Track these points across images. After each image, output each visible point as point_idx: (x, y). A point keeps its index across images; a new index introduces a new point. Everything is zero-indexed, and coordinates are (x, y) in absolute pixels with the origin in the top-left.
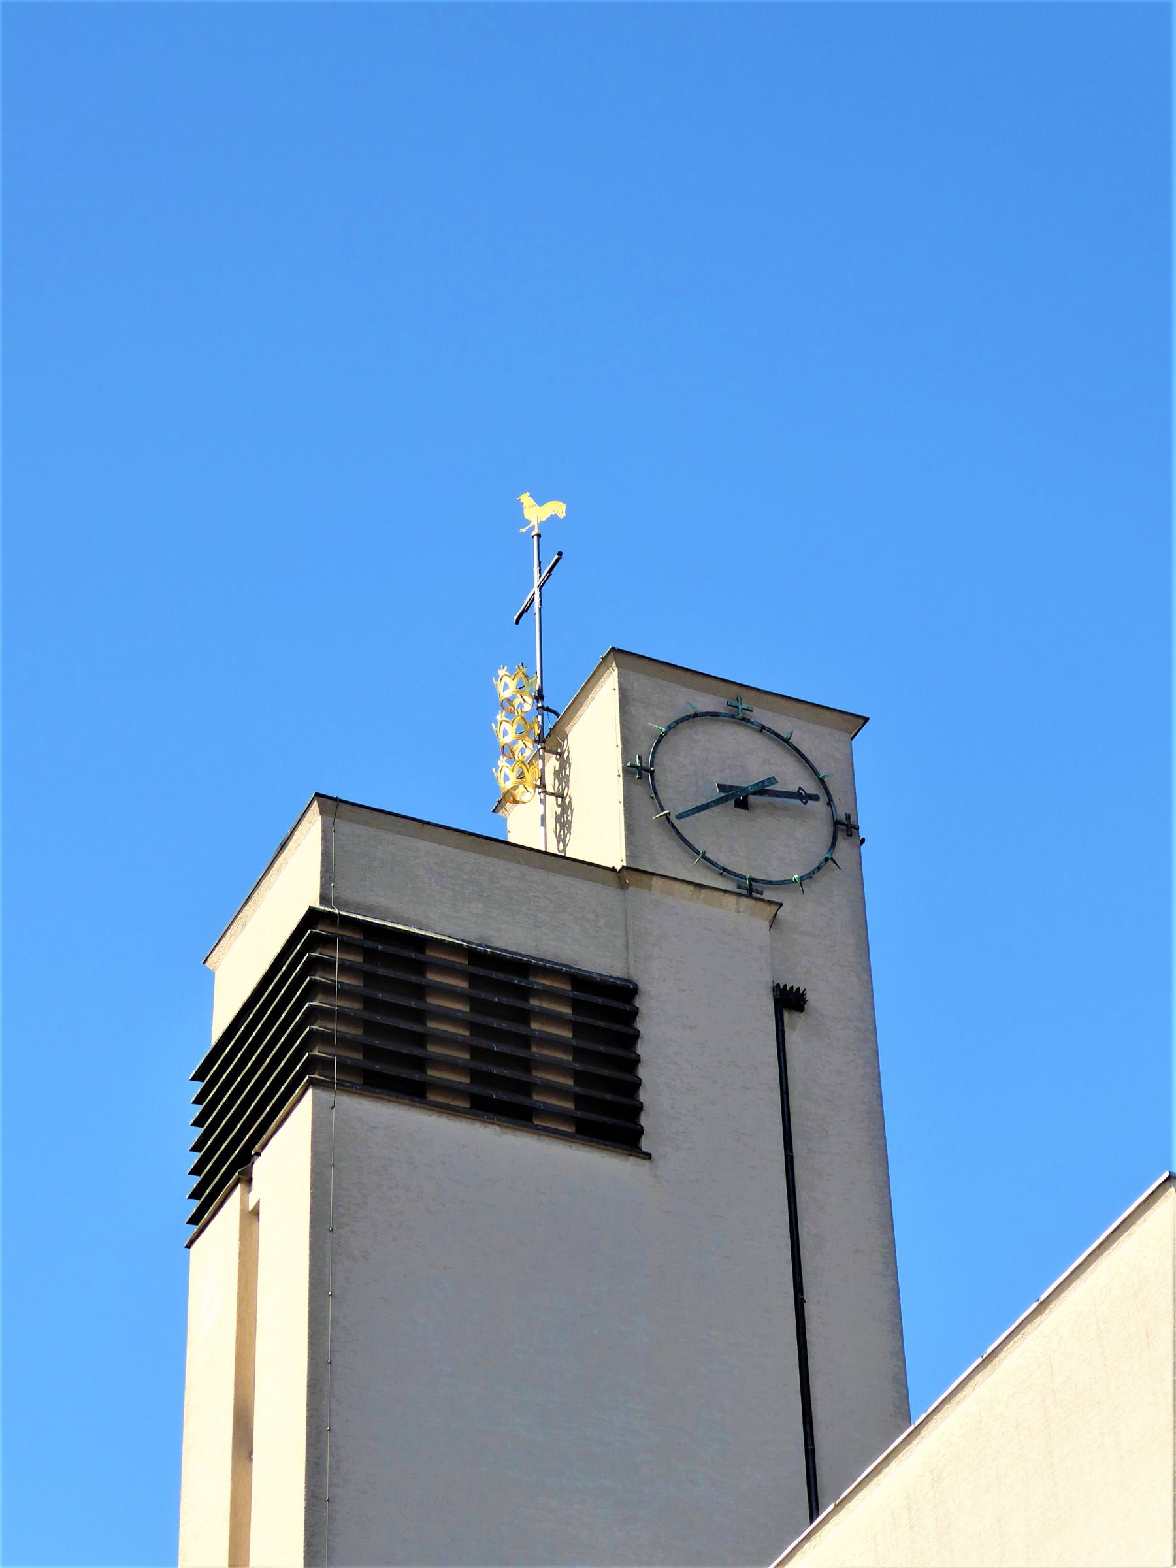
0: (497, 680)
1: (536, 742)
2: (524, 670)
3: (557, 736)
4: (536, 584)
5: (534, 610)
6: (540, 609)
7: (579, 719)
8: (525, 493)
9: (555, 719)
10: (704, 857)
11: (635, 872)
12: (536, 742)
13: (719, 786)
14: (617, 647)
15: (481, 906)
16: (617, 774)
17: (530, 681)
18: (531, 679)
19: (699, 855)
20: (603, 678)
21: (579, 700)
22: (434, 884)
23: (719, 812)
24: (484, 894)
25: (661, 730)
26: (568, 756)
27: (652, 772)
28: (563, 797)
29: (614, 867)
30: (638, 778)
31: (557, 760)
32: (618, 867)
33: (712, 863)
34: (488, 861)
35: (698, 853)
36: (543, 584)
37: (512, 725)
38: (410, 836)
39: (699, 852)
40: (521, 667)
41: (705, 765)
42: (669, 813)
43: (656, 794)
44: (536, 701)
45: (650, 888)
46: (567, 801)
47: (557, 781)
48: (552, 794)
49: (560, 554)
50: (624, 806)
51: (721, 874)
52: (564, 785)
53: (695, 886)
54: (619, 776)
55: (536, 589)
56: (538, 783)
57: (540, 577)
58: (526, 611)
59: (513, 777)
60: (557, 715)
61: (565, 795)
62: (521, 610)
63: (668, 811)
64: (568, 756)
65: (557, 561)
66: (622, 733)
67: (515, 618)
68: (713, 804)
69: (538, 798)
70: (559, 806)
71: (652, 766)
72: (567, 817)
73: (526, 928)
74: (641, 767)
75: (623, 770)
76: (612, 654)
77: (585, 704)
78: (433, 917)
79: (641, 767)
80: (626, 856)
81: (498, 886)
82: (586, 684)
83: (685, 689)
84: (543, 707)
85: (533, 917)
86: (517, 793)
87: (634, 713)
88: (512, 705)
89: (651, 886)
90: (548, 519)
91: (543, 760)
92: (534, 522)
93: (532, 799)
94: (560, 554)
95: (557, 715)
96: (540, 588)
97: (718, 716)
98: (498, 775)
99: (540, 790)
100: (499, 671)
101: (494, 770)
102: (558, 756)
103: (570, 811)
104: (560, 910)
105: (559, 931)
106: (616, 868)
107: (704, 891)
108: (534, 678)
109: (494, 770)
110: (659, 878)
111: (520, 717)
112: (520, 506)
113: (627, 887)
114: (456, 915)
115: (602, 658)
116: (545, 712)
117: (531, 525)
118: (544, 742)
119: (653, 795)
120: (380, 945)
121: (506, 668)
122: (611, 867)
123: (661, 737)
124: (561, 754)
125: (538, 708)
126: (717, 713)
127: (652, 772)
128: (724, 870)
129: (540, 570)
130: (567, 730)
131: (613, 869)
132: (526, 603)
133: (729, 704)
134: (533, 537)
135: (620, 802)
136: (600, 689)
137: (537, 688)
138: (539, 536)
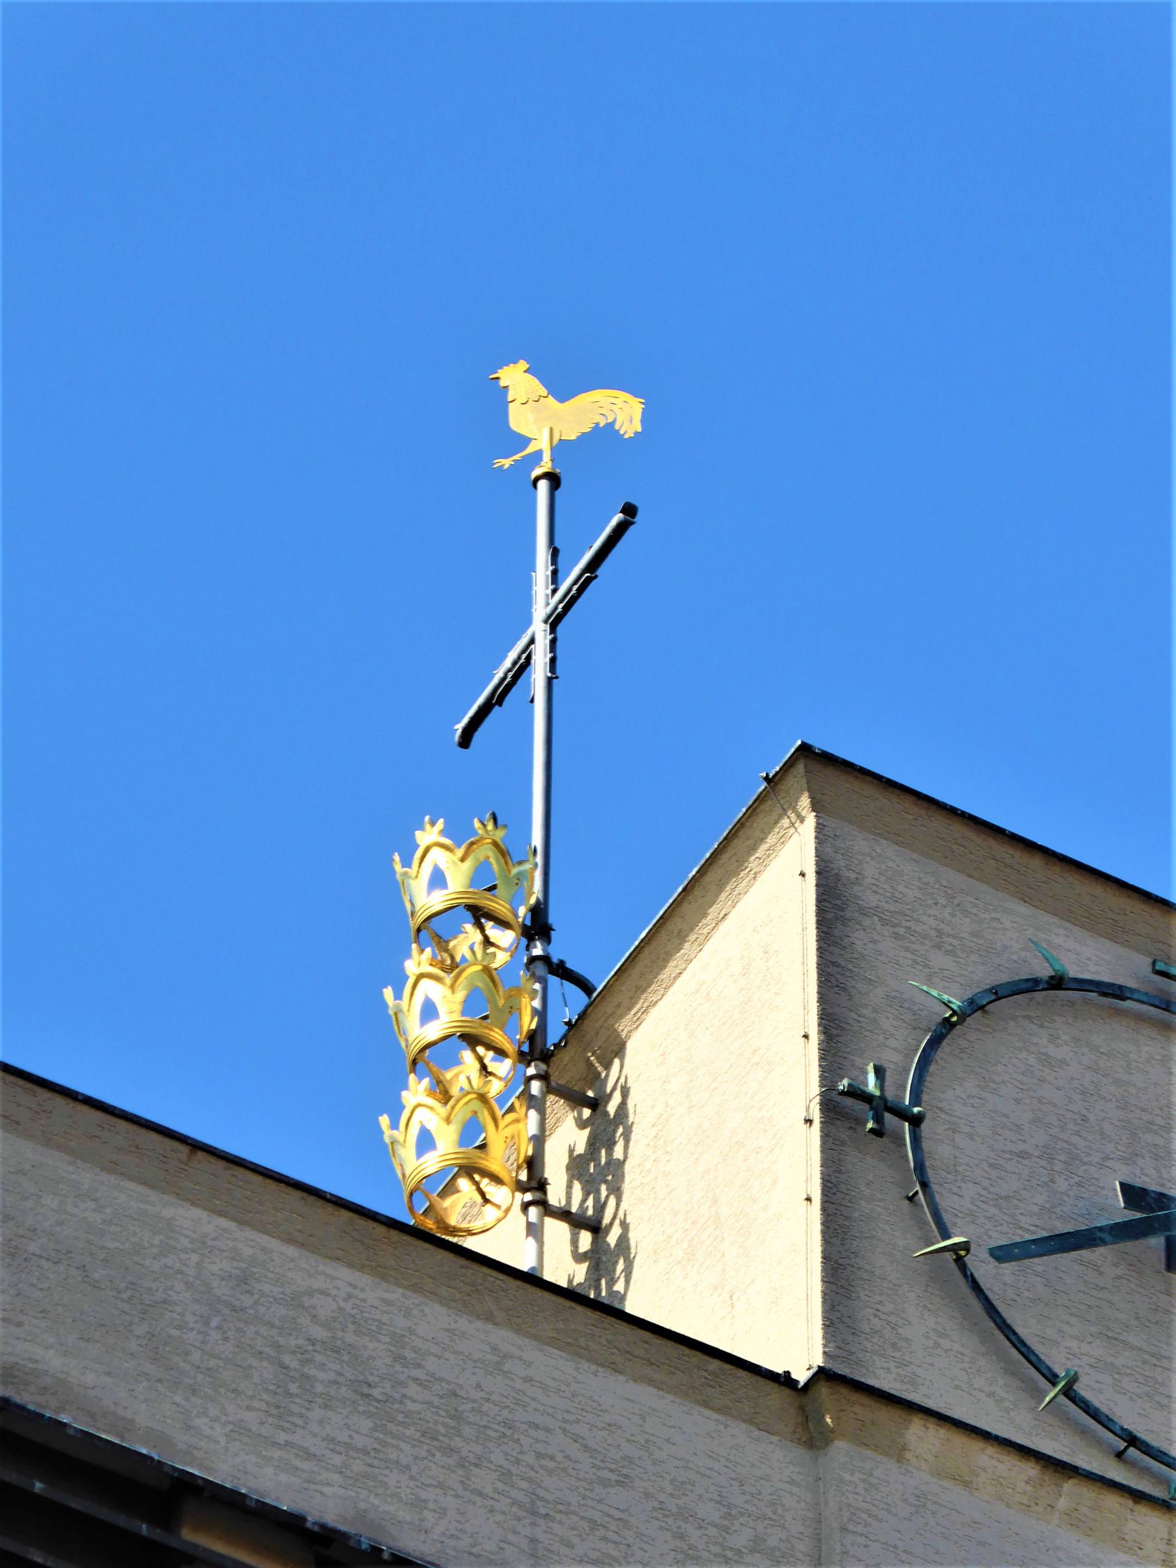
0: (407, 863)
1: (524, 1058)
2: (499, 835)
3: (585, 1050)
4: (542, 602)
5: (528, 686)
6: (549, 681)
7: (667, 988)
8: (515, 362)
9: (579, 999)
10: (1068, 1392)
11: (854, 1396)
12: (524, 1058)
13: (1126, 1188)
14: (820, 743)
15: (366, 1424)
16: (803, 1115)
17: (515, 871)
18: (520, 863)
19: (1054, 1384)
20: (764, 847)
21: (675, 924)
22: (215, 1335)
23: (1119, 1277)
24: (376, 1392)
25: (947, 1005)
26: (623, 1106)
27: (916, 1122)
28: (596, 1228)
29: (787, 1373)
30: (872, 1131)
31: (581, 1124)
32: (801, 1376)
33: (1094, 1414)
34: (389, 1296)
35: (1052, 1379)
36: (567, 609)
37: (452, 987)
38: (152, 1187)
39: (1056, 1376)
40: (490, 826)
41: (1077, 1134)
42: (966, 1246)
43: (924, 1185)
44: (524, 941)
45: (899, 1453)
46: (612, 1239)
47: (577, 1186)
48: (564, 1215)
49: (630, 510)
50: (824, 1209)
51: (1120, 1455)
52: (604, 1193)
53: (1045, 1467)
54: (809, 1121)
55: (539, 629)
56: (523, 1176)
57: (554, 591)
58: (500, 702)
59: (447, 1141)
60: (585, 986)
61: (606, 1220)
62: (481, 700)
63: (963, 1239)
64: (623, 1106)
65: (620, 531)
66: (822, 998)
67: (460, 727)
68: (1106, 1237)
69: (517, 1220)
70: (578, 1257)
71: (916, 1099)
72: (612, 1282)
73: (503, 1513)
74: (882, 1098)
75: (821, 1104)
76: (800, 767)
77: (692, 937)
78: (208, 1431)
79: (882, 1098)
80: (825, 1353)
81: (420, 1374)
82: (702, 871)
83: (1024, 909)
84: (545, 959)
85: (524, 1485)
86: (453, 1205)
87: (859, 946)
88: (446, 950)
89: (904, 1448)
90: (583, 437)
91: (542, 1113)
92: (541, 443)
93: (499, 1221)
94: (630, 510)
95: (585, 986)
96: (554, 622)
97: (1123, 999)
98: (398, 1135)
99: (528, 1197)
100: (418, 833)
101: (384, 1121)
102: (587, 1113)
103: (621, 1266)
104: (613, 1477)
105: (605, 1539)
106: (794, 1376)
107: (1070, 1486)
108: (527, 866)
109: (384, 1121)
110: (932, 1425)
111: (479, 968)
112: (500, 398)
113: (827, 1442)
114: (282, 1437)
115: (767, 779)
116: (553, 980)
117: (530, 449)
118: (546, 1057)
119: (918, 1188)
120: (41, 1481)
121: (440, 824)
122: (779, 1370)
123: (947, 1025)
124: (595, 1105)
125: (533, 960)
126: (1120, 987)
127: (916, 1122)
128: (1132, 1440)
129: (555, 573)
130: (623, 1027)
131: (786, 1380)
132: (499, 674)
133: (1160, 966)
134: (535, 482)
135: (808, 1199)
136: (749, 886)
137: (533, 901)
138: (554, 479)
